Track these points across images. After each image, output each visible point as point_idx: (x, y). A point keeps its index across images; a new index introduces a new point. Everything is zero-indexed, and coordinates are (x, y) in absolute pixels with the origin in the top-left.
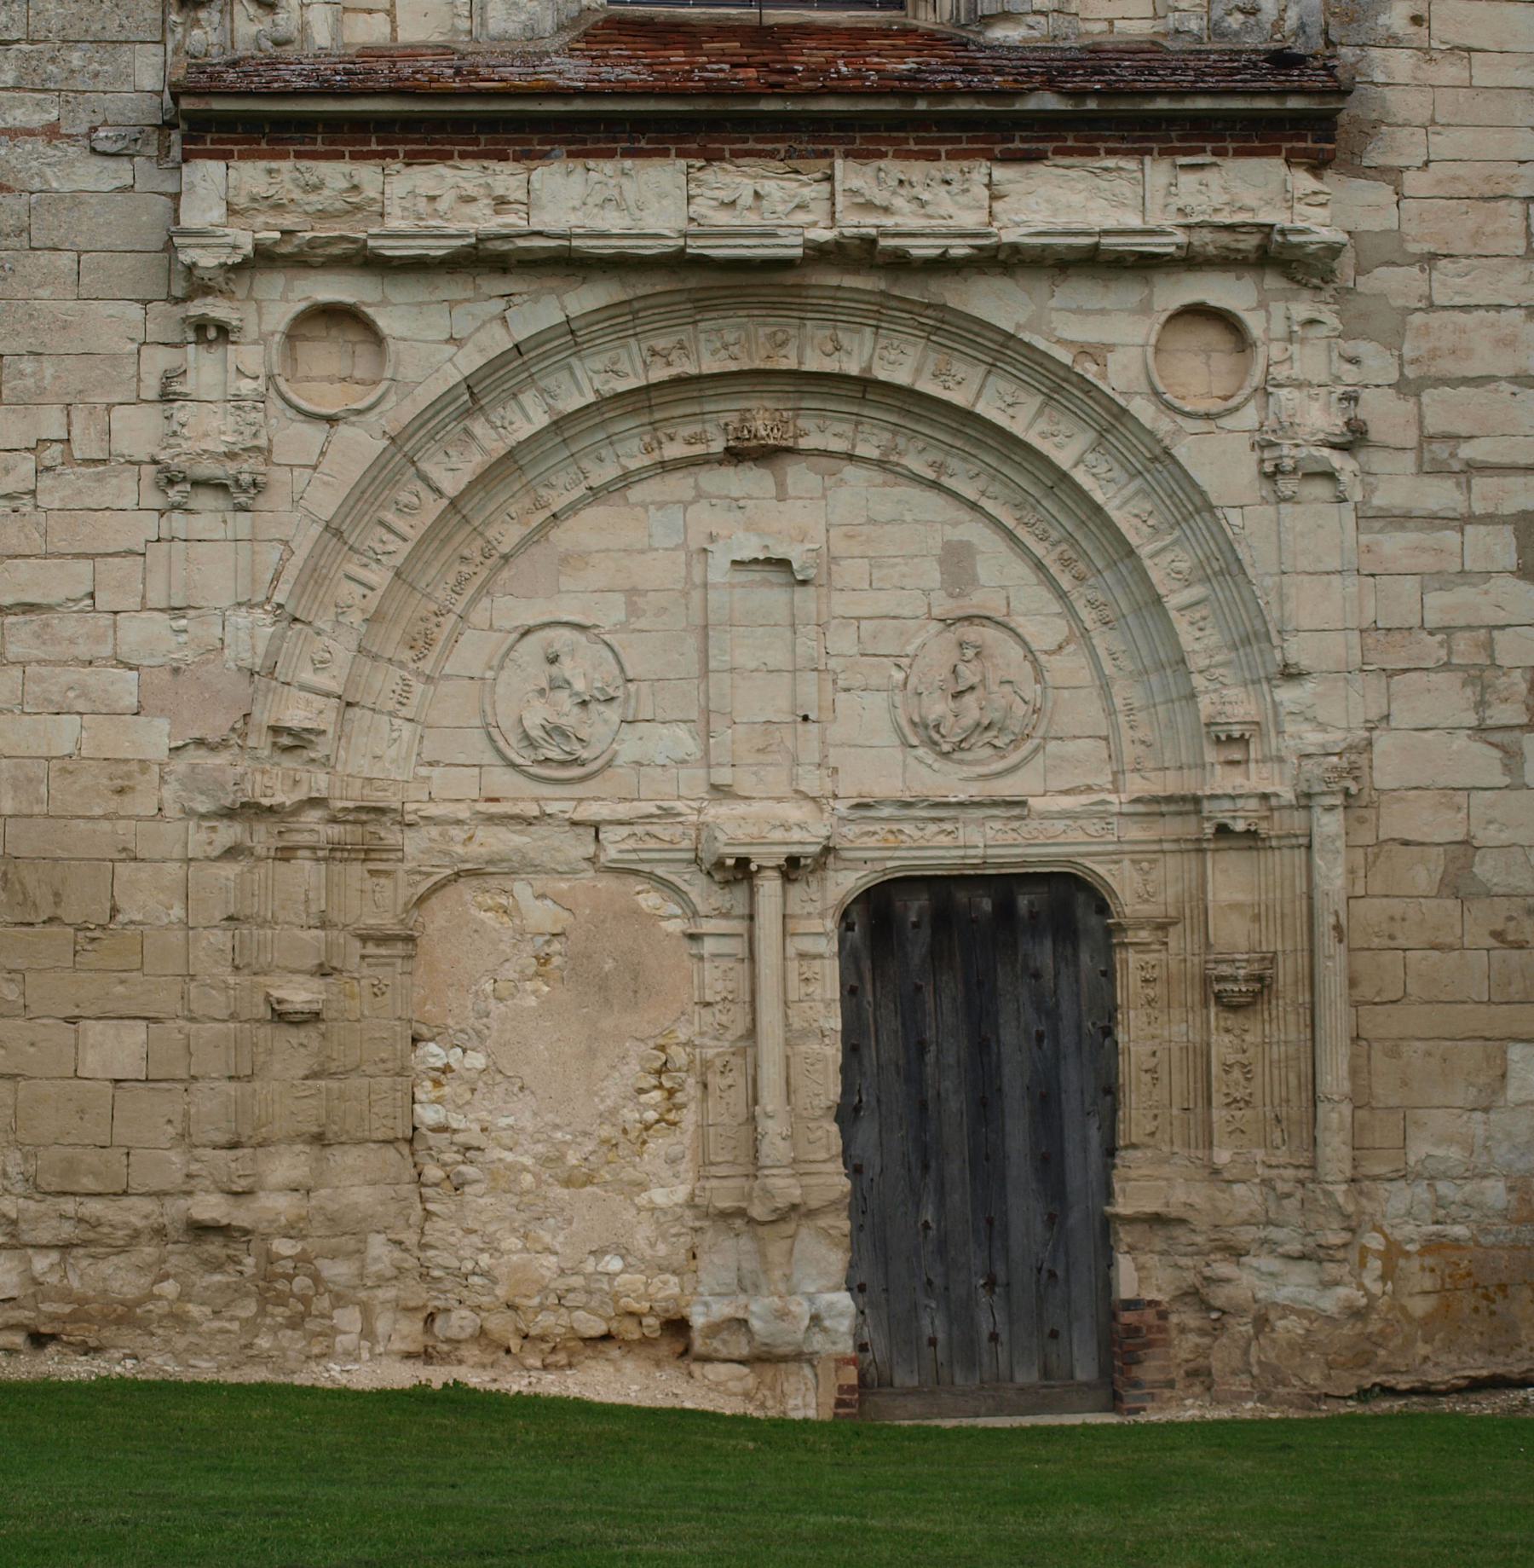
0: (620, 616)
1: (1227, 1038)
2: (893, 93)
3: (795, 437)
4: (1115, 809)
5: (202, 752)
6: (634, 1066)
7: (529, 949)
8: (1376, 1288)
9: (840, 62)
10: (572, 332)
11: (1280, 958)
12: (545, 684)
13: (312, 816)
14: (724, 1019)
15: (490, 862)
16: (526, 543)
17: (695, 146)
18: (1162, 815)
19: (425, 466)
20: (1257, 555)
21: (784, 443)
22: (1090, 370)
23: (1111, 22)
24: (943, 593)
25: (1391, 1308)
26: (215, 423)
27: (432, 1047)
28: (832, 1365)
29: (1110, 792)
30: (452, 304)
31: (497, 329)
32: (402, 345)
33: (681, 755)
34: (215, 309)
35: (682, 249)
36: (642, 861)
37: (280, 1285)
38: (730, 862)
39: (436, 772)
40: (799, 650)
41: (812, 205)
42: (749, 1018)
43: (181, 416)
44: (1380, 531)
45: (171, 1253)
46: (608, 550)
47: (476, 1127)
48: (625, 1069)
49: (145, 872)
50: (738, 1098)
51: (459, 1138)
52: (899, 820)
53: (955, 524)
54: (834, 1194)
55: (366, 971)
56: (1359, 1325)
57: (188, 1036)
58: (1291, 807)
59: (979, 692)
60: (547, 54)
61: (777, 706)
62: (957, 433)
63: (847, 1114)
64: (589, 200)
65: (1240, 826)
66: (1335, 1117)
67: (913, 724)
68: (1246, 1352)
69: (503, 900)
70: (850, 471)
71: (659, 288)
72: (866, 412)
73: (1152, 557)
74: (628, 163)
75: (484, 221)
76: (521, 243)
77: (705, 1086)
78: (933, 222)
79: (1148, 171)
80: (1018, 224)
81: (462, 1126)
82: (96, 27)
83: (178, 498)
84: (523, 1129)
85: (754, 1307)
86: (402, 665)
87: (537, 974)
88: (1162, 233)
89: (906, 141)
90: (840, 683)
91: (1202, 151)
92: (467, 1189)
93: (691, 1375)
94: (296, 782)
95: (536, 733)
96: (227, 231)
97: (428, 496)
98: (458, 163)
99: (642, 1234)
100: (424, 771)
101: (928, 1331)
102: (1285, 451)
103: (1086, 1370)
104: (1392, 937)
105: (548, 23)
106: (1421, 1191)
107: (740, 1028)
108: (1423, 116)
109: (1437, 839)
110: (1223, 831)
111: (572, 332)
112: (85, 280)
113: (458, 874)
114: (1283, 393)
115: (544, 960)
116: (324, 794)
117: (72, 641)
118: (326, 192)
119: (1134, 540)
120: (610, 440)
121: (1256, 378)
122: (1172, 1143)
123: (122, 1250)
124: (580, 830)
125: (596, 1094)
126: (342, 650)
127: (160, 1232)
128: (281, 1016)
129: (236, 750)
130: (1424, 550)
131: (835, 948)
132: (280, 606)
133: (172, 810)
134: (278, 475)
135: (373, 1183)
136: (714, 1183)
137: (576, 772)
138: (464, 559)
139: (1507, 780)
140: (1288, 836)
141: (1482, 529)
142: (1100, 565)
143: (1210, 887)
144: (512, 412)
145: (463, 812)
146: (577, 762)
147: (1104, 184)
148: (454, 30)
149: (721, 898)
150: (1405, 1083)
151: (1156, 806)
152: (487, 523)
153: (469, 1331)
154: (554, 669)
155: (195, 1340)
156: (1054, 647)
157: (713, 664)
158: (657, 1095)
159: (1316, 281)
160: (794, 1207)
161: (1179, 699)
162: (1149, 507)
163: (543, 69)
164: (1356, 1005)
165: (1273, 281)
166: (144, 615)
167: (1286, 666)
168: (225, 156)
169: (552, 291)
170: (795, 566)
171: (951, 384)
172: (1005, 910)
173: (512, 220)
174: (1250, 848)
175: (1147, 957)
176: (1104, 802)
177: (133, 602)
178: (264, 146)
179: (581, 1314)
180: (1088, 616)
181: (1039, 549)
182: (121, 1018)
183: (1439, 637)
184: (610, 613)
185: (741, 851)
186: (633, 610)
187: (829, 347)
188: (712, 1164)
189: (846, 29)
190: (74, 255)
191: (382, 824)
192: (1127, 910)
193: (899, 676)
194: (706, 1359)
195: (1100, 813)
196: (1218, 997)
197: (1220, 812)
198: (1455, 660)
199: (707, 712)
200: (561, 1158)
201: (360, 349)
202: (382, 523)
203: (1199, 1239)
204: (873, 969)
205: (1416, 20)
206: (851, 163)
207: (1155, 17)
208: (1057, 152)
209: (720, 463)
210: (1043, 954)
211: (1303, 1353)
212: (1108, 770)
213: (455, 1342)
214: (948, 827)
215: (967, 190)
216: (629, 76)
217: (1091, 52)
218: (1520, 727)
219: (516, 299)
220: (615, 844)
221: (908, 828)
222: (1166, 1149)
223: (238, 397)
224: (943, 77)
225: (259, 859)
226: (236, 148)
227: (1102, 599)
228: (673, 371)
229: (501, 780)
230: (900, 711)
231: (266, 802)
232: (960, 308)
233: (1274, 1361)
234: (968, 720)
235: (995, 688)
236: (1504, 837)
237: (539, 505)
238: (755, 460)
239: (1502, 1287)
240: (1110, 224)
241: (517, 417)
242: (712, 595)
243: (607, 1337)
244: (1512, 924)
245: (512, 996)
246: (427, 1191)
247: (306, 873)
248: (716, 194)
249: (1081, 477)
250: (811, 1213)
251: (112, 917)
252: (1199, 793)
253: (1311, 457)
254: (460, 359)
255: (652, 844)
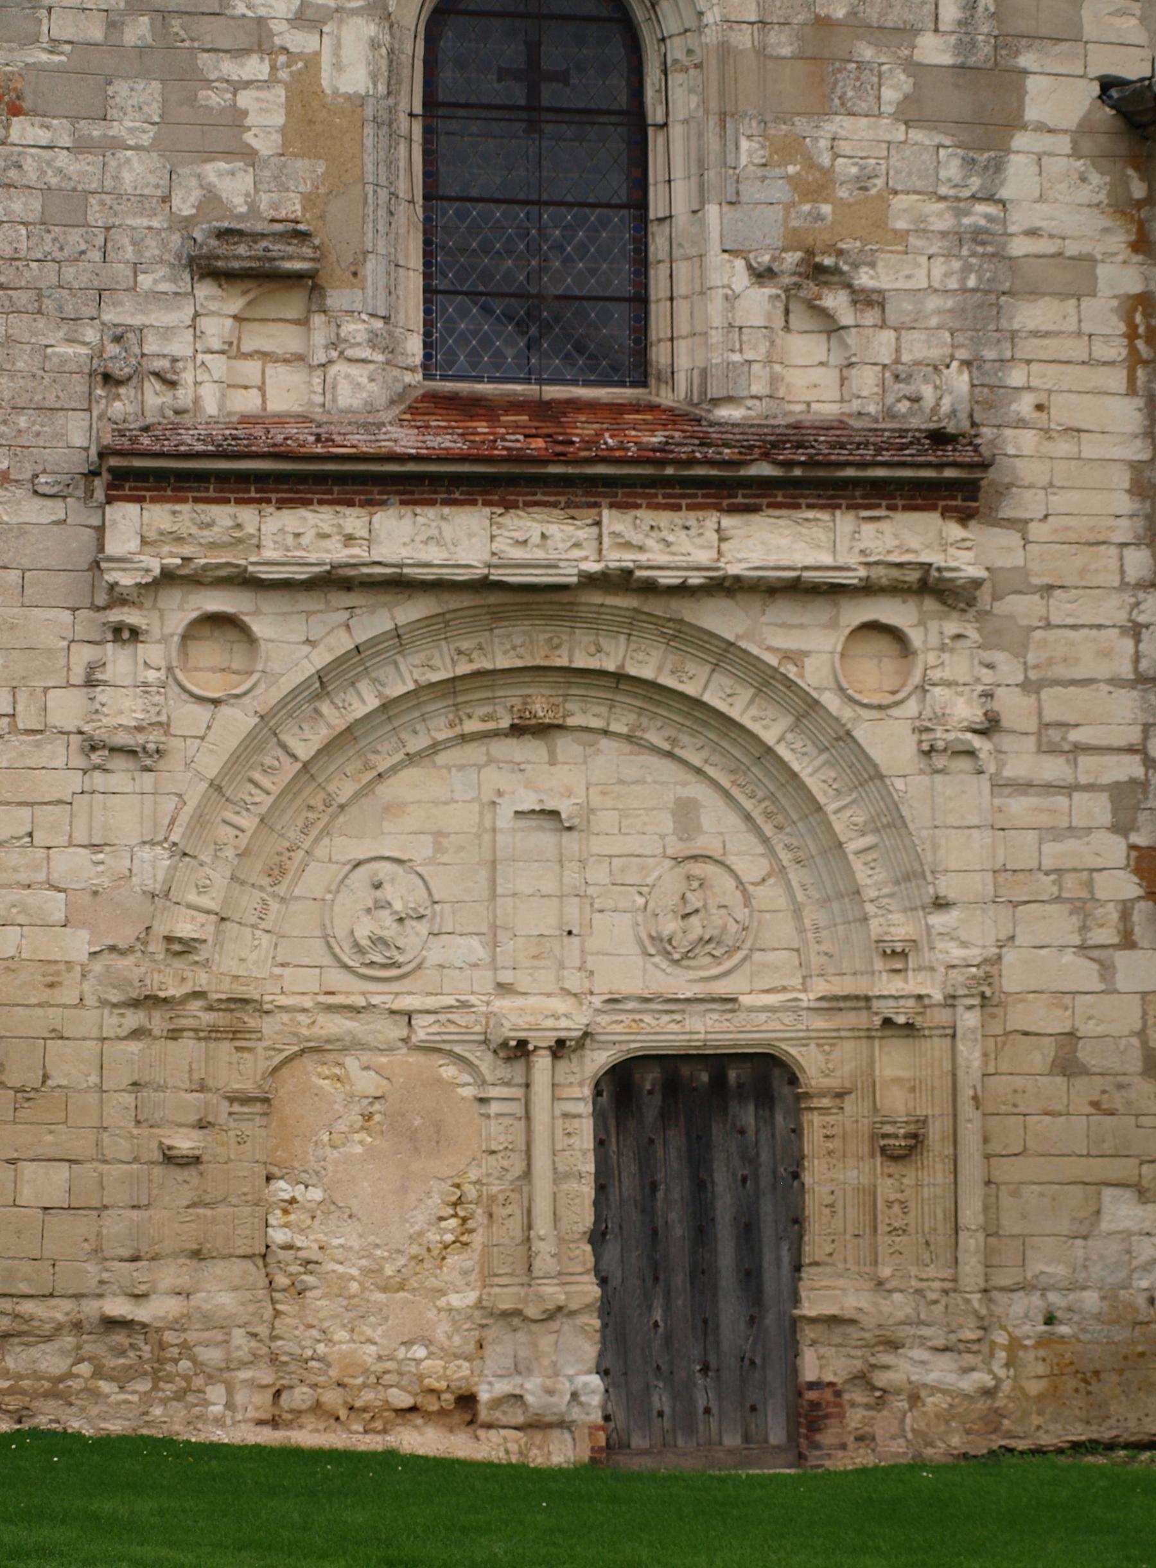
0: (428, 852)
1: (889, 1181)
2: (649, 461)
3: (564, 717)
4: (805, 1004)
5: (114, 956)
6: (436, 1199)
7: (356, 1109)
8: (1002, 1373)
9: (607, 435)
10: (399, 636)
11: (930, 1120)
12: (370, 904)
13: (196, 1005)
14: (505, 1163)
15: (328, 1041)
16: (358, 795)
17: (496, 497)
18: (840, 1009)
19: (285, 737)
20: (916, 813)
21: (556, 722)
22: (791, 671)
23: (808, 404)
24: (674, 838)
25: (1013, 1389)
26: (127, 703)
27: (282, 1184)
28: (586, 1431)
29: (800, 991)
30: (309, 614)
31: (342, 633)
32: (270, 645)
33: (474, 960)
34: (131, 616)
35: (486, 577)
36: (444, 1041)
37: (169, 1367)
38: (513, 1043)
39: (287, 971)
40: (566, 881)
41: (585, 544)
42: (524, 1164)
43: (102, 698)
44: (1009, 796)
45: (86, 1342)
46: (419, 802)
47: (315, 1246)
48: (430, 1202)
49: (68, 1047)
50: (515, 1226)
51: (301, 1254)
52: (640, 1012)
53: (685, 784)
54: (589, 1300)
55: (232, 1124)
56: (989, 1402)
57: (101, 1175)
58: (940, 1005)
59: (702, 914)
60: (383, 424)
61: (548, 923)
62: (688, 715)
63: (597, 1237)
64: (417, 539)
65: (901, 1020)
66: (970, 1242)
67: (652, 938)
68: (902, 1421)
69: (337, 1071)
70: (605, 743)
71: (466, 604)
72: (618, 698)
73: (836, 812)
74: (446, 510)
75: (336, 553)
76: (365, 570)
77: (491, 1215)
78: (677, 558)
79: (838, 521)
80: (740, 561)
81: (304, 1245)
82: (38, 397)
83: (98, 761)
84: (351, 1248)
85: (528, 1386)
86: (262, 888)
87: (363, 1128)
88: (849, 569)
89: (656, 495)
90: (596, 906)
91: (879, 506)
92: (308, 1294)
93: (477, 1438)
94: (183, 979)
95: (364, 942)
96: (142, 558)
97: (286, 760)
98: (316, 507)
99: (441, 1330)
100: (278, 971)
101: (657, 1405)
102: (938, 735)
103: (777, 1435)
104: (1015, 1105)
105: (382, 400)
106: (1035, 1299)
107: (518, 1169)
108: (1044, 480)
109: (1050, 1031)
110: (888, 1022)
111: (399, 636)
112: (28, 592)
113: (303, 1051)
114: (937, 691)
115: (368, 1117)
116: (205, 989)
117: (15, 870)
118: (216, 529)
119: (822, 799)
120: (423, 718)
121: (916, 679)
122: (845, 1261)
123: (48, 1339)
124: (397, 1017)
125: (407, 1221)
126: (219, 877)
127: (77, 1326)
128: (170, 1159)
129: (139, 954)
130: (1042, 811)
131: (590, 1109)
132: (175, 844)
133: (91, 1000)
134: (177, 743)
135: (235, 1289)
136: (497, 1290)
137: (394, 972)
138: (310, 808)
139: (1102, 987)
140: (937, 1028)
141: (1086, 796)
142: (795, 817)
143: (877, 1065)
144: (351, 697)
145: (307, 1002)
146: (395, 965)
147: (804, 531)
148: (310, 403)
149: (504, 1071)
150: (1024, 1217)
151: (834, 1003)
152: (328, 780)
153: (309, 1403)
154: (378, 893)
155: (105, 1408)
156: (759, 879)
157: (500, 890)
158: (453, 1222)
159: (962, 605)
160: (560, 1309)
161: (855, 921)
162: (833, 774)
163: (383, 437)
164: (987, 1157)
165: (930, 604)
166: (71, 850)
167: (937, 898)
168: (140, 500)
169: (385, 605)
170: (564, 816)
171: (685, 679)
172: (719, 1081)
173: (357, 552)
174: (907, 1036)
175: (827, 1118)
176: (796, 999)
177: (62, 840)
178: (169, 493)
179: (394, 1390)
180: (785, 857)
181: (748, 805)
182: (49, 1160)
183: (1053, 877)
184: (420, 851)
185: (522, 1035)
186: (439, 848)
187: (592, 649)
188: (496, 1275)
189: (607, 405)
190: (19, 573)
191: (246, 1011)
192: (813, 1083)
193: (641, 901)
194: (489, 1426)
195: (793, 1007)
196: (883, 1149)
197: (886, 1008)
198: (1065, 895)
199: (494, 927)
200: (381, 1270)
201: (236, 646)
202: (251, 781)
203: (867, 1335)
204: (618, 1125)
205: (1039, 407)
206: (614, 512)
207: (842, 401)
208: (770, 506)
209: (506, 735)
210: (747, 1116)
211: (947, 1422)
212: (799, 975)
213: (298, 1413)
214: (678, 1017)
215: (701, 535)
216: (448, 444)
217: (795, 428)
218: (1112, 946)
219: (358, 611)
220: (423, 1030)
221: (647, 1018)
222: (840, 1265)
223: (145, 684)
224: (685, 449)
225: (156, 1038)
226: (148, 494)
227: (795, 843)
228: (475, 666)
229: (337, 978)
230: (641, 928)
231: (162, 994)
232: (693, 621)
233: (924, 1428)
234: (693, 936)
235: (714, 911)
236: (1100, 1030)
237: (368, 767)
238: (533, 734)
239: (1097, 1373)
240: (809, 561)
241: (356, 703)
242: (499, 837)
243: (413, 1409)
244: (1106, 1096)
245: (344, 1144)
246: (277, 1296)
247: (188, 1047)
248: (513, 534)
249: (782, 751)
250: (572, 1314)
251: (44, 1082)
252: (870, 994)
253: (957, 739)
254: (314, 656)
255: (452, 1028)
